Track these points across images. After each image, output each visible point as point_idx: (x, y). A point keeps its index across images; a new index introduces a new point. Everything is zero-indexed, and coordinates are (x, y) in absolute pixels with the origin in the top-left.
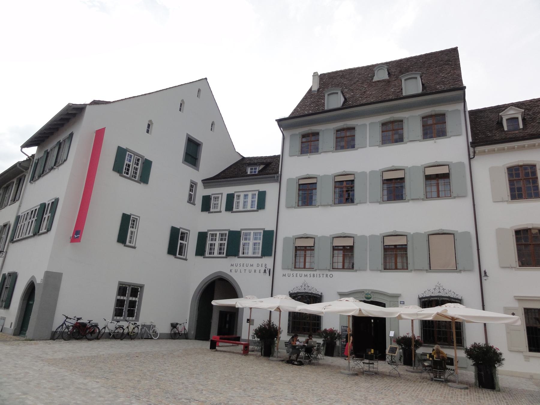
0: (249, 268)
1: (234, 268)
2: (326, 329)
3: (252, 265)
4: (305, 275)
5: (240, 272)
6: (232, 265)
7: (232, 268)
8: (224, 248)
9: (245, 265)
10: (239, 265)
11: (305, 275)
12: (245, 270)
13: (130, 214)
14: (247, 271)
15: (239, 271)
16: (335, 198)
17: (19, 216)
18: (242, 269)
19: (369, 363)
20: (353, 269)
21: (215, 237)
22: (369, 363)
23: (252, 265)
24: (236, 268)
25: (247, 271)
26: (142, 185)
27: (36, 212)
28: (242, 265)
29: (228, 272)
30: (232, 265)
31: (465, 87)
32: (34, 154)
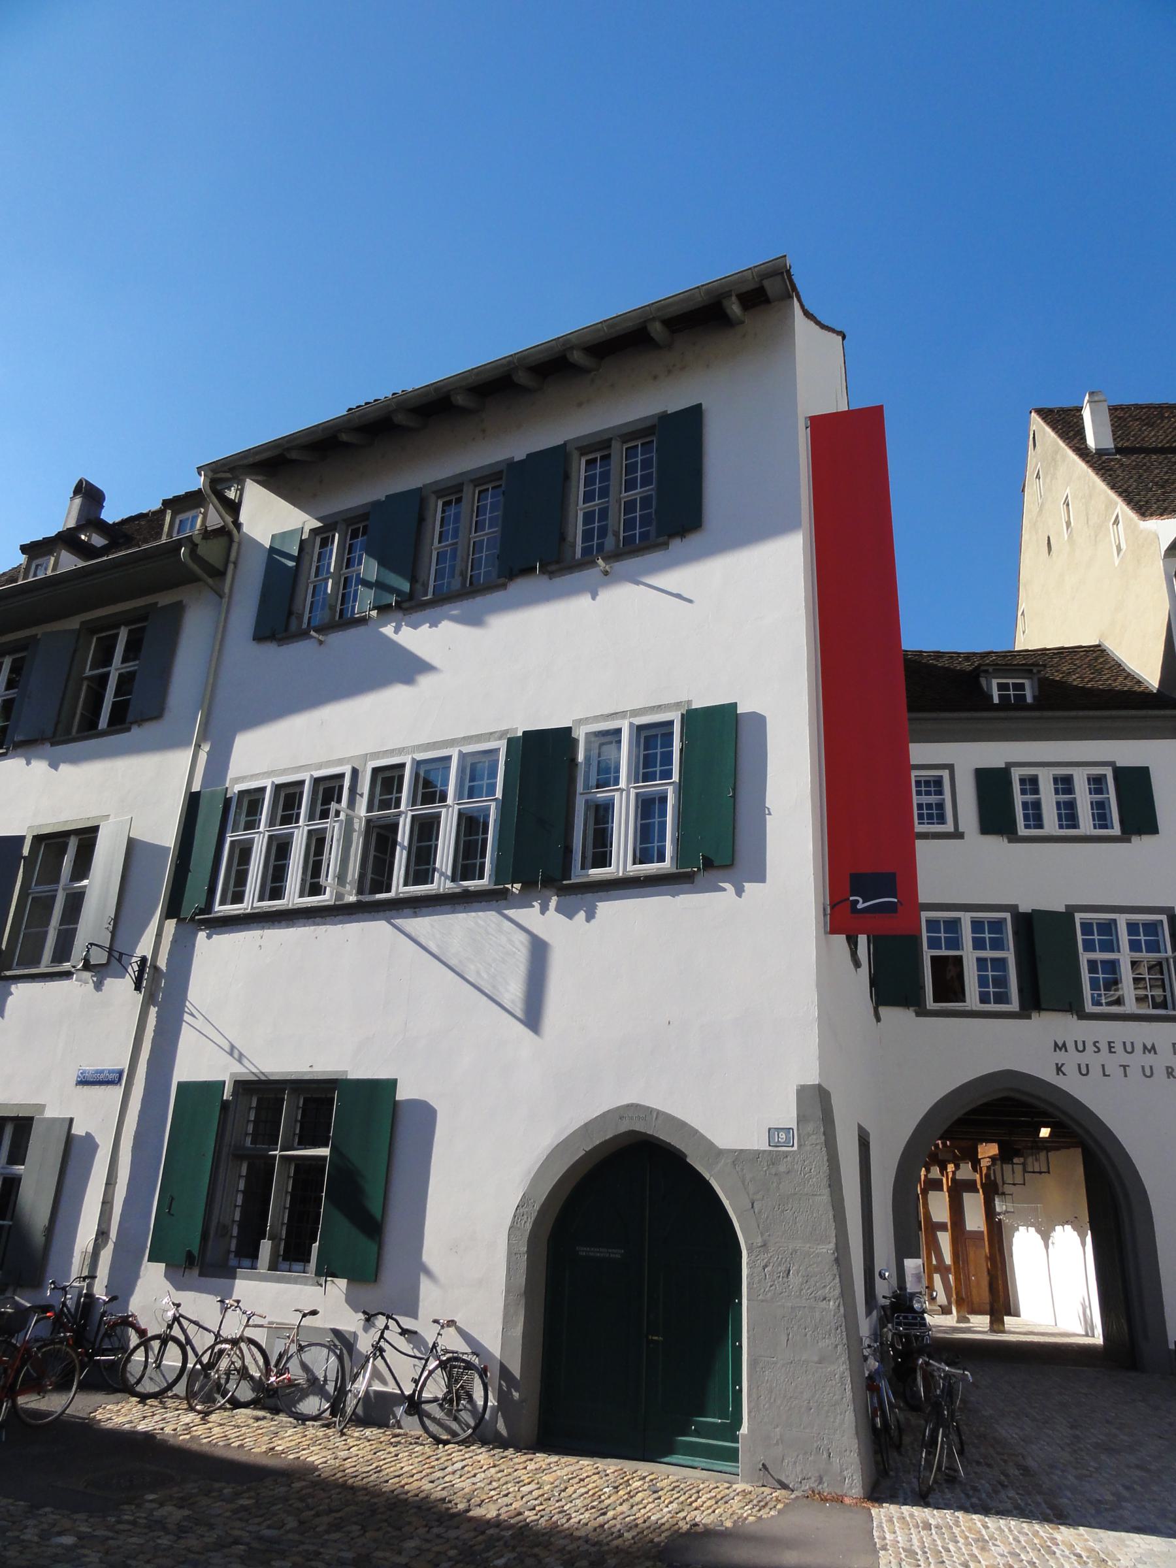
0: (1139, 1059)
1: (1070, 1059)
2: (392, 1084)
3: (1152, 1049)
4: (1145, 1047)
5: (1105, 1075)
6: (1060, 1047)
7: (1060, 1057)
8: (483, 865)
9: (1118, 1047)
10: (1090, 1048)
11: (1145, 1047)
12: (1124, 1067)
13: (1067, 906)
14: (1134, 1072)
15: (1096, 1071)
16: (732, 799)
17: (198, 794)
18: (1112, 1063)
19: (230, 1146)
20: (1093, 1005)
21: (483, 834)
22: (230, 1146)
23: (1152, 1049)
24: (1083, 1059)
25: (1134, 1072)
26: (1141, 844)
27: (598, 722)
28: (1104, 1046)
29: (1050, 1077)
30: (1060, 1047)
31: (436, 626)
32: (655, 425)
